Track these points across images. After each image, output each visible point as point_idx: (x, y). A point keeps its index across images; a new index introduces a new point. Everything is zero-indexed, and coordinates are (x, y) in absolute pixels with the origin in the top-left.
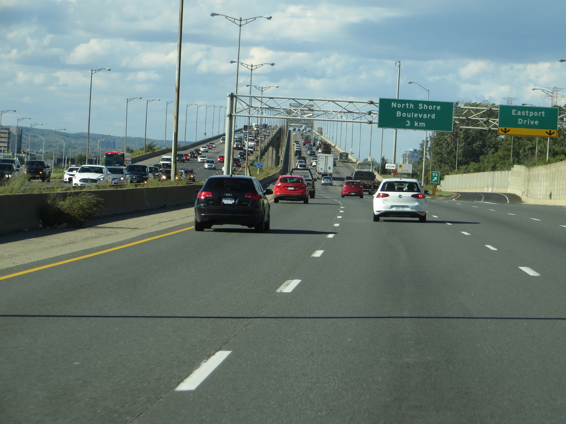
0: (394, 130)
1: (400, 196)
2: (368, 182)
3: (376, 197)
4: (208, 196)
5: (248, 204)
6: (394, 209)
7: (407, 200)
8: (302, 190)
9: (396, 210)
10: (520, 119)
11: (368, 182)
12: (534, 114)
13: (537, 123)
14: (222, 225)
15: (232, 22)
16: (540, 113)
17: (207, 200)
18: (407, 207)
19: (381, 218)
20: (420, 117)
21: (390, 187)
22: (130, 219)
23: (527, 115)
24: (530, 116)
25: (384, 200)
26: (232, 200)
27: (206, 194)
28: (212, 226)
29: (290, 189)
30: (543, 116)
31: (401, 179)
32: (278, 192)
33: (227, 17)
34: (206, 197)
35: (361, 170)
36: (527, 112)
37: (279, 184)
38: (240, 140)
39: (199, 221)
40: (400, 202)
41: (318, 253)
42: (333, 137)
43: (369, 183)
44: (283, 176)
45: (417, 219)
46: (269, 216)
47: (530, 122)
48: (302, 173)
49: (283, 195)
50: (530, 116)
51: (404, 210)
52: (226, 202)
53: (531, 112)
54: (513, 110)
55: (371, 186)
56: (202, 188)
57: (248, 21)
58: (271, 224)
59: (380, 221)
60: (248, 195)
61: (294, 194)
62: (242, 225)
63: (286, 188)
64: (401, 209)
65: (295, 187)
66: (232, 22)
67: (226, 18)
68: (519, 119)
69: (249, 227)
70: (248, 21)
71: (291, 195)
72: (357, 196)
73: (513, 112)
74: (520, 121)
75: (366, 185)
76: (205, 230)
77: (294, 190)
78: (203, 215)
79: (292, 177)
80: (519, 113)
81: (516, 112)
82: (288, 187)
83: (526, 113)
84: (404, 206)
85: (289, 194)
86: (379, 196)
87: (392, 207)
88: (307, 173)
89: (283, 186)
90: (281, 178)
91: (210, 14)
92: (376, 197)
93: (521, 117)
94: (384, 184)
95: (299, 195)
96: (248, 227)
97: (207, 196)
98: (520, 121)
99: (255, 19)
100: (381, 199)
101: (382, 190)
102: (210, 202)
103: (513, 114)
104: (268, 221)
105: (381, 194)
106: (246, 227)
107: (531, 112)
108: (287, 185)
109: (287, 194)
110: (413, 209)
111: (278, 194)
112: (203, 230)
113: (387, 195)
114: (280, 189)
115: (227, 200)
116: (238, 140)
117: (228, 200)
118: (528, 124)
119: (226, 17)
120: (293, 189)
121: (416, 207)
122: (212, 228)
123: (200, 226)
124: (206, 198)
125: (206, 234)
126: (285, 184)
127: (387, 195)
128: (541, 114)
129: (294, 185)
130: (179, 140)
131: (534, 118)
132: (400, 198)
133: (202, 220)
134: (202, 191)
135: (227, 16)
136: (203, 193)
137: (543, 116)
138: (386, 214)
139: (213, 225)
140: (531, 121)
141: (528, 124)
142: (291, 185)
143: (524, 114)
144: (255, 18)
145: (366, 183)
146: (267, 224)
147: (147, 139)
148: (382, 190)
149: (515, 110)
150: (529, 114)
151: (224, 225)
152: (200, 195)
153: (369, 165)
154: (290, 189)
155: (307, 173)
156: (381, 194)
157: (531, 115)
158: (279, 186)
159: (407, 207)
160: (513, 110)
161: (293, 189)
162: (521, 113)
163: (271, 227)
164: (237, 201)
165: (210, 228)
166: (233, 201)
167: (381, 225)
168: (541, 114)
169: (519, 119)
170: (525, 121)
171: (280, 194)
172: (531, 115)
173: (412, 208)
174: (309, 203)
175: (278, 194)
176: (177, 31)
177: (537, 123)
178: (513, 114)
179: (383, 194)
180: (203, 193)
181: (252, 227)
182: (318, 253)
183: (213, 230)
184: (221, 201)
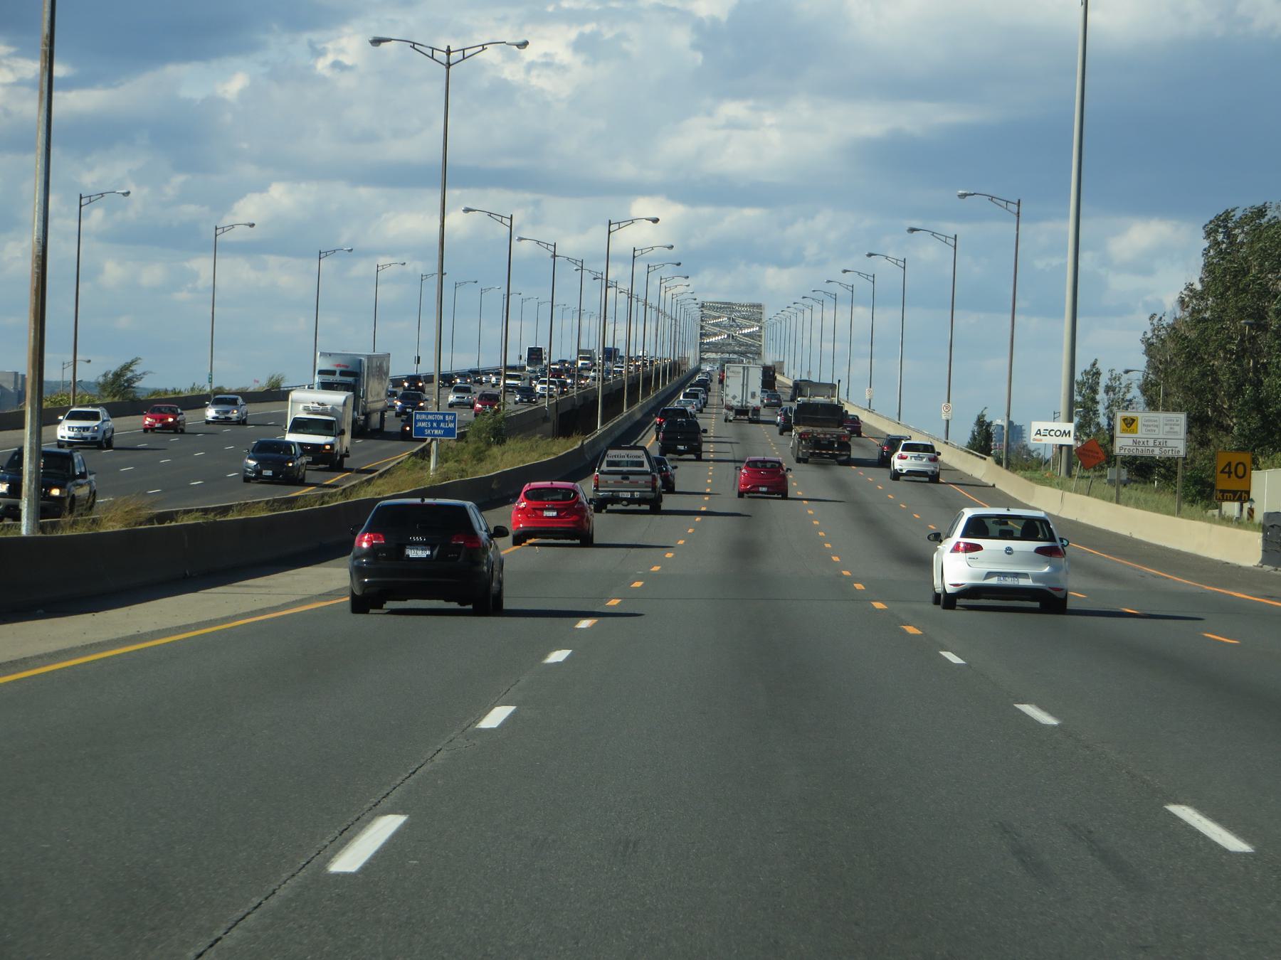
1: (1009, 551)
4: (376, 542)
5: (458, 557)
6: (994, 581)
7: (1025, 559)
8: (574, 518)
9: (999, 583)
14: (406, 600)
15: (437, 49)
17: (373, 551)
18: (1025, 575)
19: (960, 602)
21: (977, 528)
22: (506, 618)
25: (970, 558)
26: (426, 550)
27: (373, 538)
28: (385, 603)
29: (546, 514)
31: (1008, 510)
32: (520, 523)
33: (416, 46)
34: (373, 543)
37: (523, 505)
38: (350, 379)
39: (358, 593)
41: (558, 656)
44: (532, 484)
46: (500, 583)
49: (532, 529)
51: (1016, 583)
52: (413, 553)
56: (364, 527)
58: (506, 593)
59: (957, 608)
60: (459, 539)
61: (555, 525)
62: (446, 601)
63: (538, 512)
64: (1009, 582)
66: (437, 49)
67: (413, 47)
69: (461, 605)
71: (550, 529)
76: (371, 611)
78: (366, 580)
79: (553, 486)
82: (542, 510)
84: (1016, 575)
85: (547, 525)
86: (956, 549)
87: (990, 575)
88: (639, 457)
90: (527, 491)
91: (370, 39)
95: (570, 528)
96: (459, 604)
97: (374, 542)
99: (483, 49)
100: (961, 555)
102: (380, 555)
104: (500, 592)
105: (962, 545)
106: (454, 605)
109: (540, 525)
111: (521, 526)
112: (366, 612)
113: (978, 548)
114: (524, 515)
116: (337, 378)
120: (555, 514)
122: (384, 607)
123: (362, 603)
124: (372, 546)
125: (373, 621)
126: (534, 504)
127: (978, 548)
132: (1009, 554)
133: (366, 591)
134: (364, 533)
136: (366, 537)
139: (388, 602)
144: (483, 45)
146: (498, 598)
148: (964, 535)
151: (409, 601)
152: (361, 541)
154: (546, 514)
155: (639, 457)
156: (962, 545)
158: (523, 509)
159: (1025, 575)
161: (555, 514)
163: (507, 605)
164: (435, 552)
165: (381, 608)
171: (526, 527)
173: (1037, 578)
175: (521, 526)
179: (965, 543)
180: (366, 537)
181: (468, 604)
182: (558, 656)
183: (386, 611)
184: (404, 552)
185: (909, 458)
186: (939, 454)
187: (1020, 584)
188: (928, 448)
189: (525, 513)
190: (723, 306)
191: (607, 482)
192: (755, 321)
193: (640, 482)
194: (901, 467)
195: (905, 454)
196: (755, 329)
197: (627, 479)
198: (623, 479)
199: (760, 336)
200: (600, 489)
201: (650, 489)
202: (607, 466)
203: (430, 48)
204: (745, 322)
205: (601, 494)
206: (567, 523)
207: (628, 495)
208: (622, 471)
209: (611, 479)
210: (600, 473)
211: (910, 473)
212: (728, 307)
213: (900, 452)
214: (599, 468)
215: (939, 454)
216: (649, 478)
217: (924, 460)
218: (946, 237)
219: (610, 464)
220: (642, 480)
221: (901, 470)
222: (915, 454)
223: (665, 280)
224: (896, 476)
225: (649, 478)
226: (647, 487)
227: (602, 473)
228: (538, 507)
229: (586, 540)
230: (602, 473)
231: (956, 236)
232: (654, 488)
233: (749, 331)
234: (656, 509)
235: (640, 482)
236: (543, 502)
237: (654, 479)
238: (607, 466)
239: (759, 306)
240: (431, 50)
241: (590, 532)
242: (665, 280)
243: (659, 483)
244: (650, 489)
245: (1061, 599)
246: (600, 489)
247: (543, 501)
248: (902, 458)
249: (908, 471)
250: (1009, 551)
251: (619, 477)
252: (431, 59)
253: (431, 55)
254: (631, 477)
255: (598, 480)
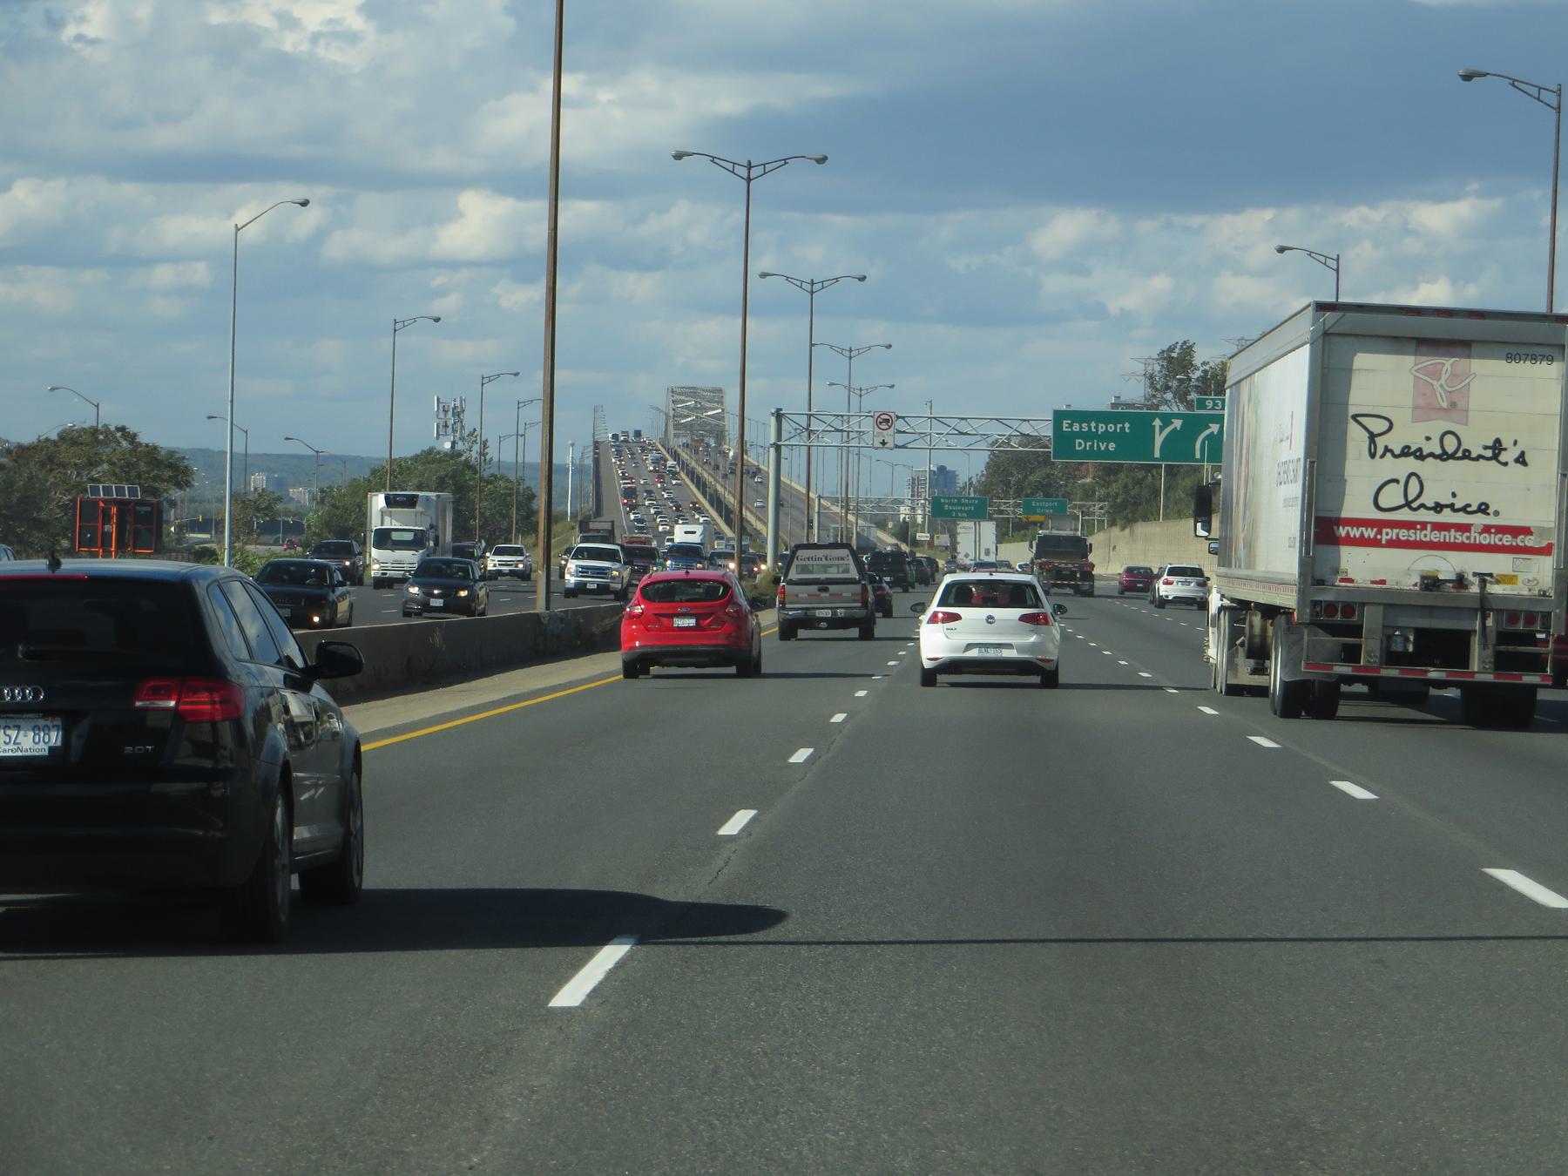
0: (1350, 406)
1: (990, 620)
2: (1066, 564)
3: (928, 623)
6: (974, 653)
10: (1081, 441)
11: (1066, 564)
12: (1106, 428)
13: (1112, 446)
15: (1544, 89)
16: (1119, 426)
18: (1009, 646)
20: (1103, 449)
21: (961, 595)
23: (1094, 430)
24: (1100, 433)
26: (47, 729)
29: (680, 622)
30: (1127, 431)
35: (1055, 532)
36: (1093, 424)
37: (638, 610)
40: (1000, 634)
42: (799, 476)
43: (1070, 566)
45: (1036, 679)
47: (1098, 444)
48: (826, 558)
49: (656, 650)
50: (1100, 433)
51: (999, 655)
53: (1100, 425)
54: (1065, 422)
55: (1076, 572)
57: (768, 167)
63: (664, 620)
64: (992, 654)
65: (698, 617)
66: (1544, 89)
68: (1077, 441)
70: (768, 167)
72: (845, 627)
73: (1065, 425)
74: (1080, 444)
75: (1061, 572)
77: (697, 628)
80: (1076, 427)
81: (1071, 426)
82: (671, 616)
83: (1090, 427)
86: (934, 619)
87: (969, 646)
88: (842, 559)
89: (655, 615)
90: (647, 585)
92: (928, 623)
93: (1080, 435)
94: (948, 587)
98: (1080, 444)
99: (786, 163)
101: (942, 603)
103: (1065, 429)
105: (940, 615)
107: (1100, 425)
108: (670, 611)
110: (1026, 653)
115: (13, 733)
117: (18, 728)
118: (1095, 449)
119: (1511, 82)
120: (691, 622)
121: (1033, 647)
126: (658, 607)
127: (956, 617)
128: (1123, 429)
129: (696, 608)
130: (554, 461)
131: (1106, 437)
132: (990, 623)
135: (1514, 80)
137: (1127, 431)
138: (952, 666)
140: (1101, 444)
141: (1095, 449)
142: (684, 610)
143: (1087, 429)
144: (785, 160)
145: (1063, 565)
147: (503, 462)
148: (942, 603)
149: (1069, 422)
150: (1097, 427)
153: (1074, 519)
154: (680, 622)
155: (842, 559)
156: (940, 615)
157: (1100, 431)
159: (1009, 646)
160: (1065, 422)
161: (691, 622)
162: (1081, 428)
166: (54, 734)
167: (950, 701)
168: (1123, 429)
169: (1077, 441)
170: (1088, 444)
172: (1100, 431)
173: (1020, 649)
174: (876, 636)
175: (637, 644)
176: (547, 171)
177: (1112, 446)
178: (1065, 429)
179: (944, 613)
185: (1175, 583)
186: (1208, 579)
187: (1004, 655)
188: (1196, 572)
189: (641, 623)
190: (1102, 428)
191: (797, 595)
192: (718, 402)
193: (844, 595)
194: (1167, 594)
195: (1171, 578)
196: (718, 411)
197: (826, 590)
198: (820, 590)
199: (723, 417)
200: (787, 606)
201: (860, 605)
202: (797, 573)
203: (1536, 86)
204: (708, 405)
205: (790, 613)
206: (717, 638)
207: (828, 614)
208: (819, 579)
209: (803, 591)
210: (788, 584)
211: (1178, 600)
212: (693, 392)
213: (1165, 576)
214: (786, 576)
215: (1208, 579)
216: (857, 588)
217: (1192, 585)
218: (1540, 88)
219: (804, 569)
220: (847, 591)
221: (1167, 596)
222: (1183, 579)
223: (760, 170)
224: (1163, 603)
225: (857, 588)
226: (855, 601)
227: (791, 583)
228: (664, 612)
229: (749, 668)
230: (791, 583)
231: (1338, 256)
232: (865, 603)
233: (714, 412)
234: (867, 634)
235: (844, 595)
236: (673, 604)
237: (864, 588)
238: (797, 573)
239: (720, 391)
240: (1537, 89)
241: (754, 653)
242: (760, 170)
243: (871, 598)
244: (860, 605)
245: (1050, 671)
246: (787, 606)
247: (673, 601)
248: (1168, 583)
249: (1174, 598)
250: (990, 620)
251: (814, 589)
252: (1536, 101)
253: (1537, 96)
254: (832, 588)
255: (784, 593)
